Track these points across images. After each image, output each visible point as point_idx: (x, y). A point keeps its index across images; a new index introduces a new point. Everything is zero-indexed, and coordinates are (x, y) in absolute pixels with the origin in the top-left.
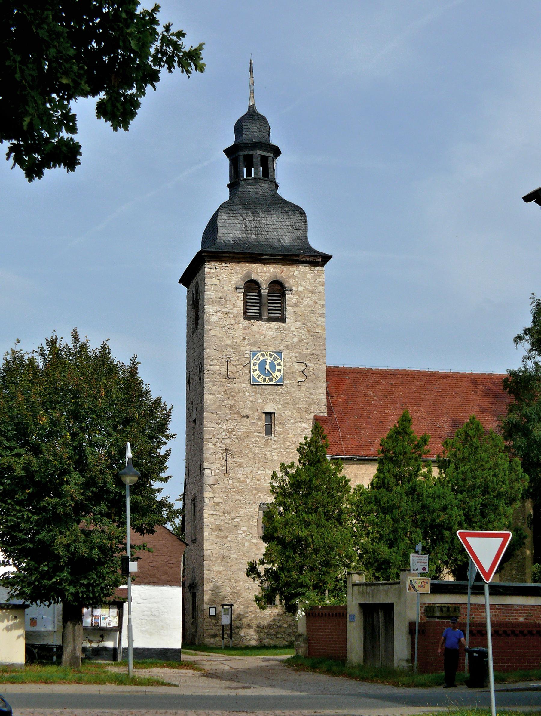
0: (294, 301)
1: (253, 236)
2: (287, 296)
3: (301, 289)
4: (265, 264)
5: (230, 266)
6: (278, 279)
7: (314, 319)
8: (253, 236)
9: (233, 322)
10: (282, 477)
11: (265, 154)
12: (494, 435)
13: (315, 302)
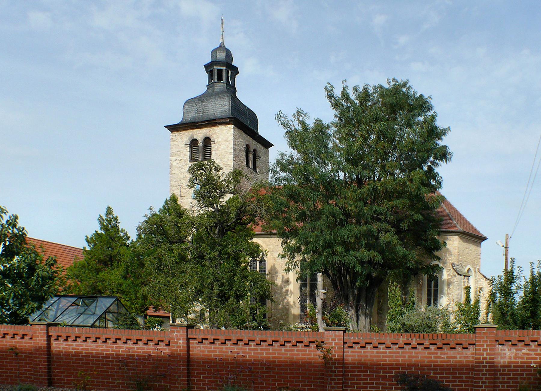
0: (216, 147)
1: (201, 114)
2: (212, 145)
3: (220, 140)
4: (200, 128)
5: (183, 132)
6: (207, 136)
7: (227, 157)
8: (201, 114)
9: (184, 164)
10: (342, 252)
11: (219, 68)
12: (173, 183)
13: (228, 147)
